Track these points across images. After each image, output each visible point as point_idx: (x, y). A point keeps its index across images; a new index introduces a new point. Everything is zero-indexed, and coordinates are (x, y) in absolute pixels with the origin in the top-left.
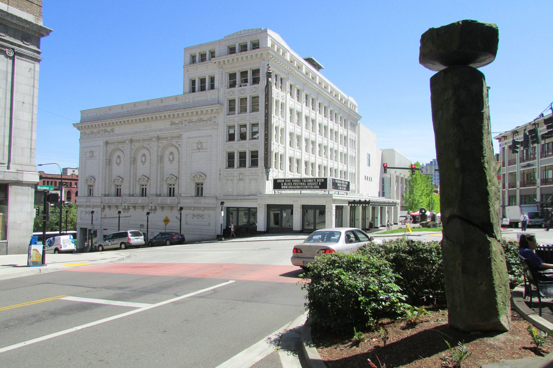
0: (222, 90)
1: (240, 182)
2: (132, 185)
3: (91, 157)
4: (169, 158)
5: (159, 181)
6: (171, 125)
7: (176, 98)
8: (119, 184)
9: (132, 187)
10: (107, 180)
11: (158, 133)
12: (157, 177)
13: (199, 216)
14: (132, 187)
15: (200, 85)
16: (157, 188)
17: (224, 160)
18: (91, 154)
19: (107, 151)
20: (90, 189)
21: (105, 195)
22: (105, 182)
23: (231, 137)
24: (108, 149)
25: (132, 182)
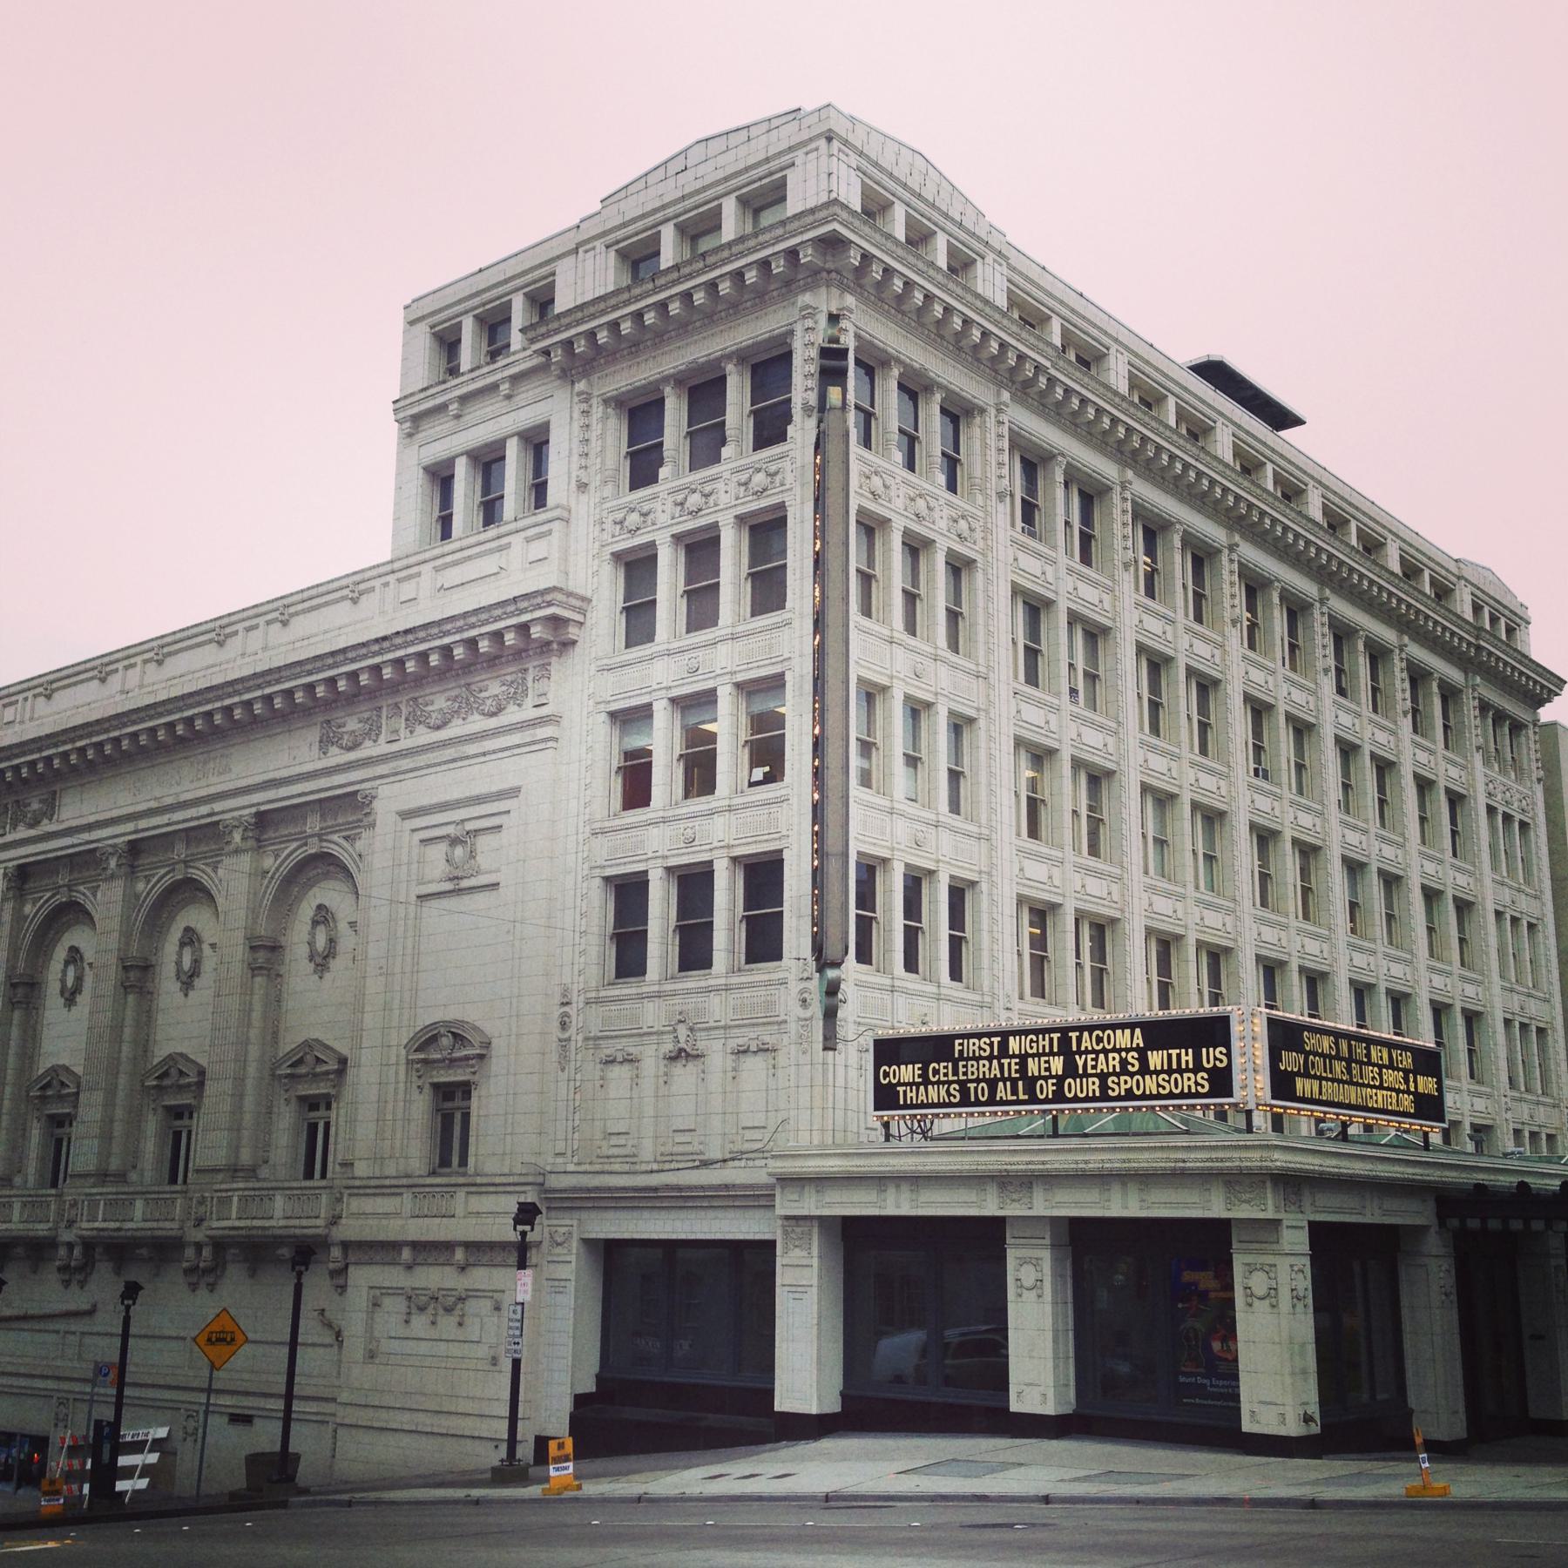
1: (678, 1069)
4: (311, 944)
7: (353, 589)
23: (635, 783)
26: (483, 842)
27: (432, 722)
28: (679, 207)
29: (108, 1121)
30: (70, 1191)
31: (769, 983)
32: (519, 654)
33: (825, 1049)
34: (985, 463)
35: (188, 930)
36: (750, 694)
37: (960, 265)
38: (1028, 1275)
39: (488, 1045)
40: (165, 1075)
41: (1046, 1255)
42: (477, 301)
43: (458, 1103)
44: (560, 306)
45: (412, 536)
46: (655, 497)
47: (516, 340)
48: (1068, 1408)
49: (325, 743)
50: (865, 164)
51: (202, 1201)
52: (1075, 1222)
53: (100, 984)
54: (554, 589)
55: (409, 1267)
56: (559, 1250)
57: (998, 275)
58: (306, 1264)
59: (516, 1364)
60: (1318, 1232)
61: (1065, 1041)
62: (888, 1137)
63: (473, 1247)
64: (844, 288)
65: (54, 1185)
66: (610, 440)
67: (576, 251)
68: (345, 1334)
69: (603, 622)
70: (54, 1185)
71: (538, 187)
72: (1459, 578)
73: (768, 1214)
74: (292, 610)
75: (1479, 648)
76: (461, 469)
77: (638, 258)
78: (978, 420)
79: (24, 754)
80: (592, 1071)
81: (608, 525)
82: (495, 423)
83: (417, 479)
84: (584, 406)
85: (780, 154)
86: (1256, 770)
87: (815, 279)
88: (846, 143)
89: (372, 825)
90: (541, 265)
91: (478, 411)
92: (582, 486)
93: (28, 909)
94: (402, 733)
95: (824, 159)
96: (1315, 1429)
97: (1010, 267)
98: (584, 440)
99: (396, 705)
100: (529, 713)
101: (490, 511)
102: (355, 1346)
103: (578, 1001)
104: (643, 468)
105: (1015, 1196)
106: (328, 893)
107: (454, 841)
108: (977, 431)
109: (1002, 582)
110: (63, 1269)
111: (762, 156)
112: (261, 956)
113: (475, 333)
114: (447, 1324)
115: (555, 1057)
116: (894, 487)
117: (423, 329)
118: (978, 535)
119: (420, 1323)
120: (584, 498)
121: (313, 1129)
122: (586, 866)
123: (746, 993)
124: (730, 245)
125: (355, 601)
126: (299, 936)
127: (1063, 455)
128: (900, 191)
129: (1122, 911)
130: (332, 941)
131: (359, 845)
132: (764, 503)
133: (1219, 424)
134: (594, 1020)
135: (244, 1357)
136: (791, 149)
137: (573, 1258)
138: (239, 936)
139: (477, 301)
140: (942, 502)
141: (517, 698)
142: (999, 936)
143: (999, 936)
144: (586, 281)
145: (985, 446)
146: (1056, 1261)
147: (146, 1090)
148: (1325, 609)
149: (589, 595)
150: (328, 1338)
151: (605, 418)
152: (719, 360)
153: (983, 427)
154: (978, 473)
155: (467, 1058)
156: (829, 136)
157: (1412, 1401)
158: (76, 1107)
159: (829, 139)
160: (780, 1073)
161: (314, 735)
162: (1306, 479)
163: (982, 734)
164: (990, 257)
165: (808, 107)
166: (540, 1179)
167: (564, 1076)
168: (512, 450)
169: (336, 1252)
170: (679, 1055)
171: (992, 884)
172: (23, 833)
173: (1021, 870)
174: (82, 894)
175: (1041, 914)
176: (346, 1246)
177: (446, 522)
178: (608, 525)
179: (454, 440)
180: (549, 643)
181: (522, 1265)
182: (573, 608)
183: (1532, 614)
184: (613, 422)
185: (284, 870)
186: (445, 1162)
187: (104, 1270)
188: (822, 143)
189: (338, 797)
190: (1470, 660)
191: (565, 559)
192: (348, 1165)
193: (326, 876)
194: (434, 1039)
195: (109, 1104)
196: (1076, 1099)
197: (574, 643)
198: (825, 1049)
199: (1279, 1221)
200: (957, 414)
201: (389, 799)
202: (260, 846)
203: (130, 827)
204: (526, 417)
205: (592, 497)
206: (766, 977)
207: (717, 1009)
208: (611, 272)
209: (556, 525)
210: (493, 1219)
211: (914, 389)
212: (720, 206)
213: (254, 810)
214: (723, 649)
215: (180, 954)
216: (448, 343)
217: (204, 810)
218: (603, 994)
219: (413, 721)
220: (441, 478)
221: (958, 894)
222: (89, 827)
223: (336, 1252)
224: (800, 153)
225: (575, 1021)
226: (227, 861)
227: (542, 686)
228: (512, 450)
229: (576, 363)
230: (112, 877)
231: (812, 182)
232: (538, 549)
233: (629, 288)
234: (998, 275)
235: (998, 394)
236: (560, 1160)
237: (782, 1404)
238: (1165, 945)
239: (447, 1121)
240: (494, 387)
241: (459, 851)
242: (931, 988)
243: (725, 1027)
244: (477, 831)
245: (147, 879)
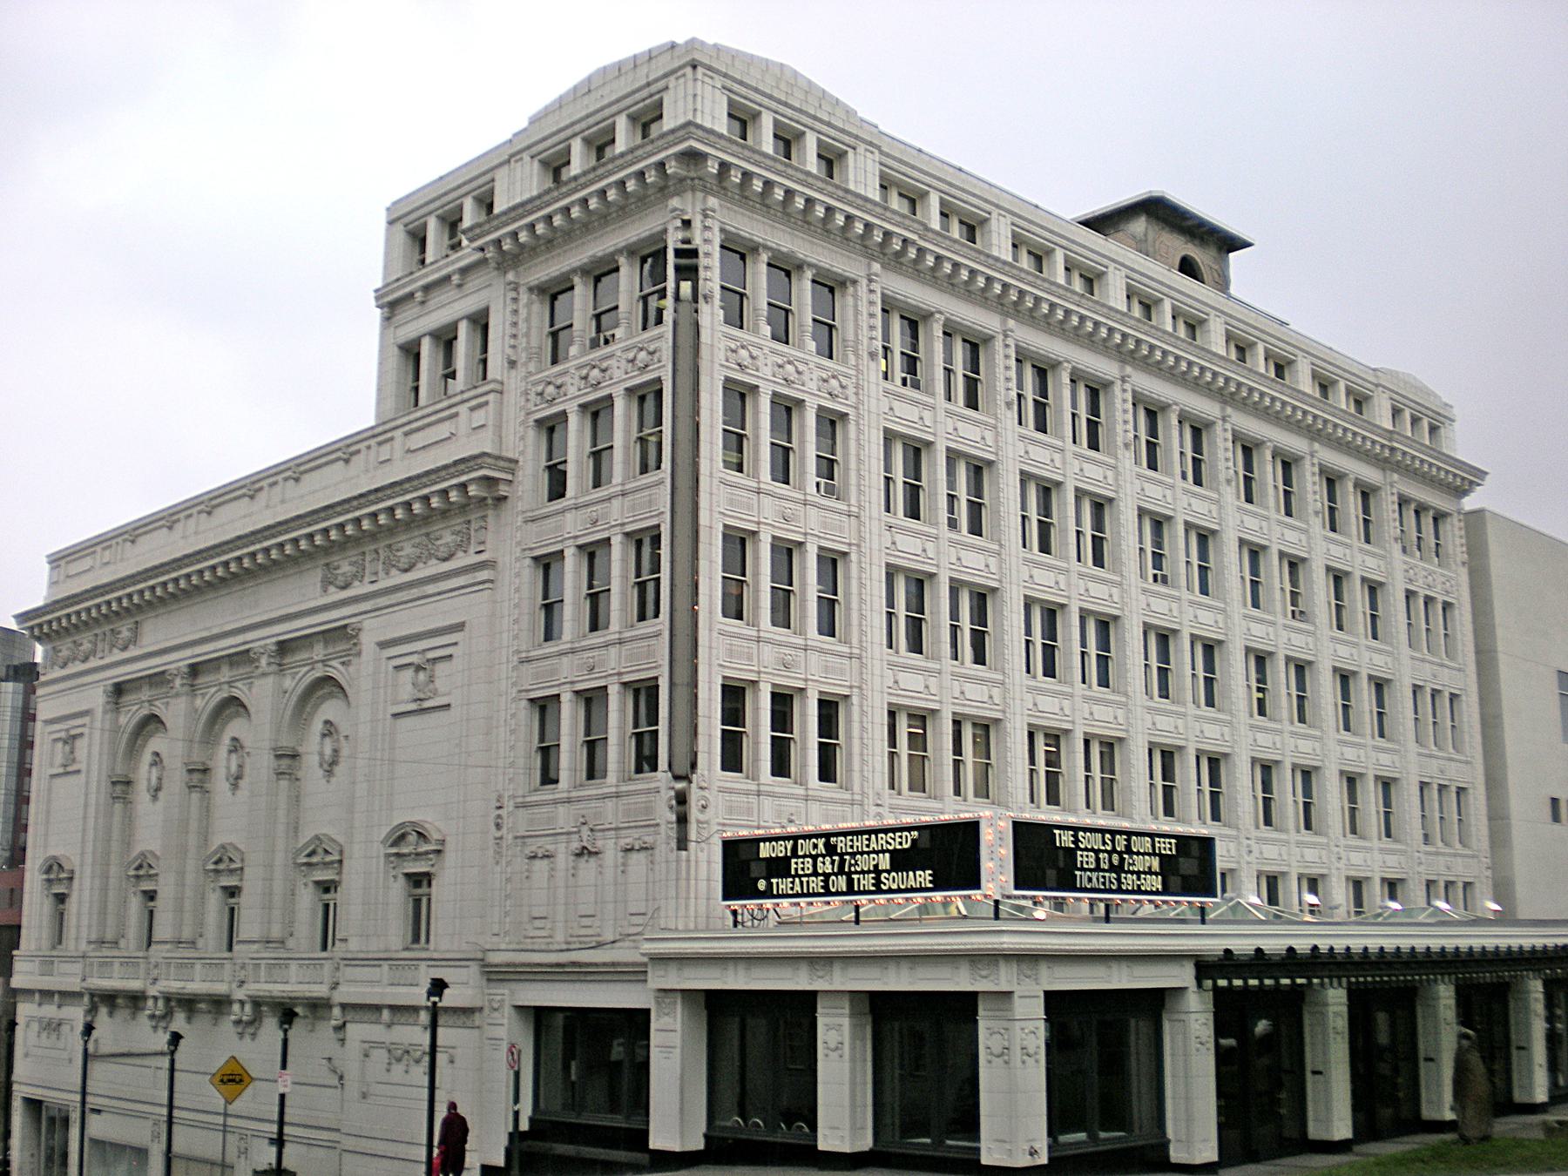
7: (344, 451)
19: (116, 729)
22: (105, 877)
26: (441, 668)
27: (440, 555)
28: (583, 125)
31: (648, 792)
32: (463, 508)
33: (679, 849)
34: (857, 326)
35: (235, 739)
37: (831, 160)
39: (443, 842)
40: (140, 867)
42: (438, 204)
46: (565, 373)
49: (327, 583)
50: (729, 83)
52: (874, 996)
53: (261, 764)
54: (484, 454)
55: (389, 1026)
56: (496, 1014)
57: (869, 162)
58: (290, 1023)
60: (1054, 1001)
62: (736, 923)
63: (63, 994)
64: (707, 191)
66: (535, 322)
67: (508, 161)
68: (346, 1077)
69: (530, 481)
71: (476, 106)
72: (1377, 385)
73: (639, 986)
74: (302, 468)
75: (1392, 449)
76: (426, 347)
77: (555, 167)
78: (851, 290)
79: (112, 591)
80: (520, 863)
81: (532, 397)
82: (451, 308)
84: (513, 294)
85: (657, 80)
86: (1155, 576)
87: (682, 185)
88: (710, 68)
89: (359, 654)
90: (484, 174)
91: (438, 298)
92: (512, 364)
93: (123, 720)
94: (382, 574)
95: (690, 84)
97: (881, 152)
98: (515, 321)
99: (376, 551)
100: (474, 559)
103: (509, 806)
105: (984, 973)
106: (331, 709)
107: (419, 668)
108: (850, 300)
109: (874, 431)
111: (644, 82)
112: (285, 762)
113: (438, 227)
115: (491, 852)
116: (761, 358)
117: (399, 227)
118: (851, 391)
119: (398, 1069)
120: (513, 372)
122: (515, 690)
123: (632, 800)
124: (622, 155)
125: (347, 461)
126: (313, 747)
127: (940, 313)
128: (766, 101)
129: (1004, 712)
130: (336, 751)
131: (351, 669)
133: (1111, 269)
134: (519, 822)
136: (666, 76)
137: (505, 1021)
138: (267, 744)
139: (438, 204)
140: (812, 365)
141: (462, 546)
144: (518, 186)
145: (857, 312)
146: (854, 1026)
147: (207, 871)
148: (1228, 426)
149: (516, 456)
151: (529, 304)
152: (613, 254)
153: (855, 297)
154: (851, 336)
155: (427, 853)
156: (691, 61)
157: (1170, 1133)
158: (340, 873)
159: (694, 67)
160: (657, 867)
161: (317, 575)
162: (1207, 309)
163: (854, 567)
164: (861, 148)
165: (680, 40)
166: (480, 955)
167: (498, 869)
168: (463, 329)
169: (336, 1011)
170: (583, 852)
171: (862, 697)
172: (118, 656)
173: (896, 682)
176: (344, 1006)
178: (532, 397)
179: (420, 323)
180: (485, 499)
182: (502, 470)
183: (1456, 412)
184: (536, 307)
185: (299, 690)
186: (416, 939)
188: (689, 70)
189: (335, 629)
190: (1386, 460)
191: (499, 427)
193: (331, 695)
194: (403, 837)
195: (181, 884)
196: (890, 891)
197: (505, 498)
198: (679, 849)
200: (830, 285)
201: (373, 631)
202: (282, 669)
203: (188, 652)
204: (470, 304)
205: (521, 371)
206: (646, 786)
207: (610, 813)
208: (535, 179)
209: (491, 397)
211: (785, 268)
212: (569, 147)
213: (274, 640)
214: (616, 503)
215: (228, 760)
216: (419, 239)
218: (574, 794)
219: (389, 565)
220: (411, 352)
221: (829, 710)
223: (336, 1011)
224: (672, 78)
225: (507, 823)
226: (257, 682)
227: (481, 535)
228: (463, 329)
229: (509, 259)
230: (177, 695)
231: (681, 103)
232: (479, 417)
233: (594, 169)
234: (869, 162)
235: (869, 266)
236: (495, 939)
237: (655, 1143)
239: (417, 902)
240: (447, 278)
241: (422, 676)
242: (800, 791)
243: (617, 829)
244: (435, 660)
245: (203, 695)
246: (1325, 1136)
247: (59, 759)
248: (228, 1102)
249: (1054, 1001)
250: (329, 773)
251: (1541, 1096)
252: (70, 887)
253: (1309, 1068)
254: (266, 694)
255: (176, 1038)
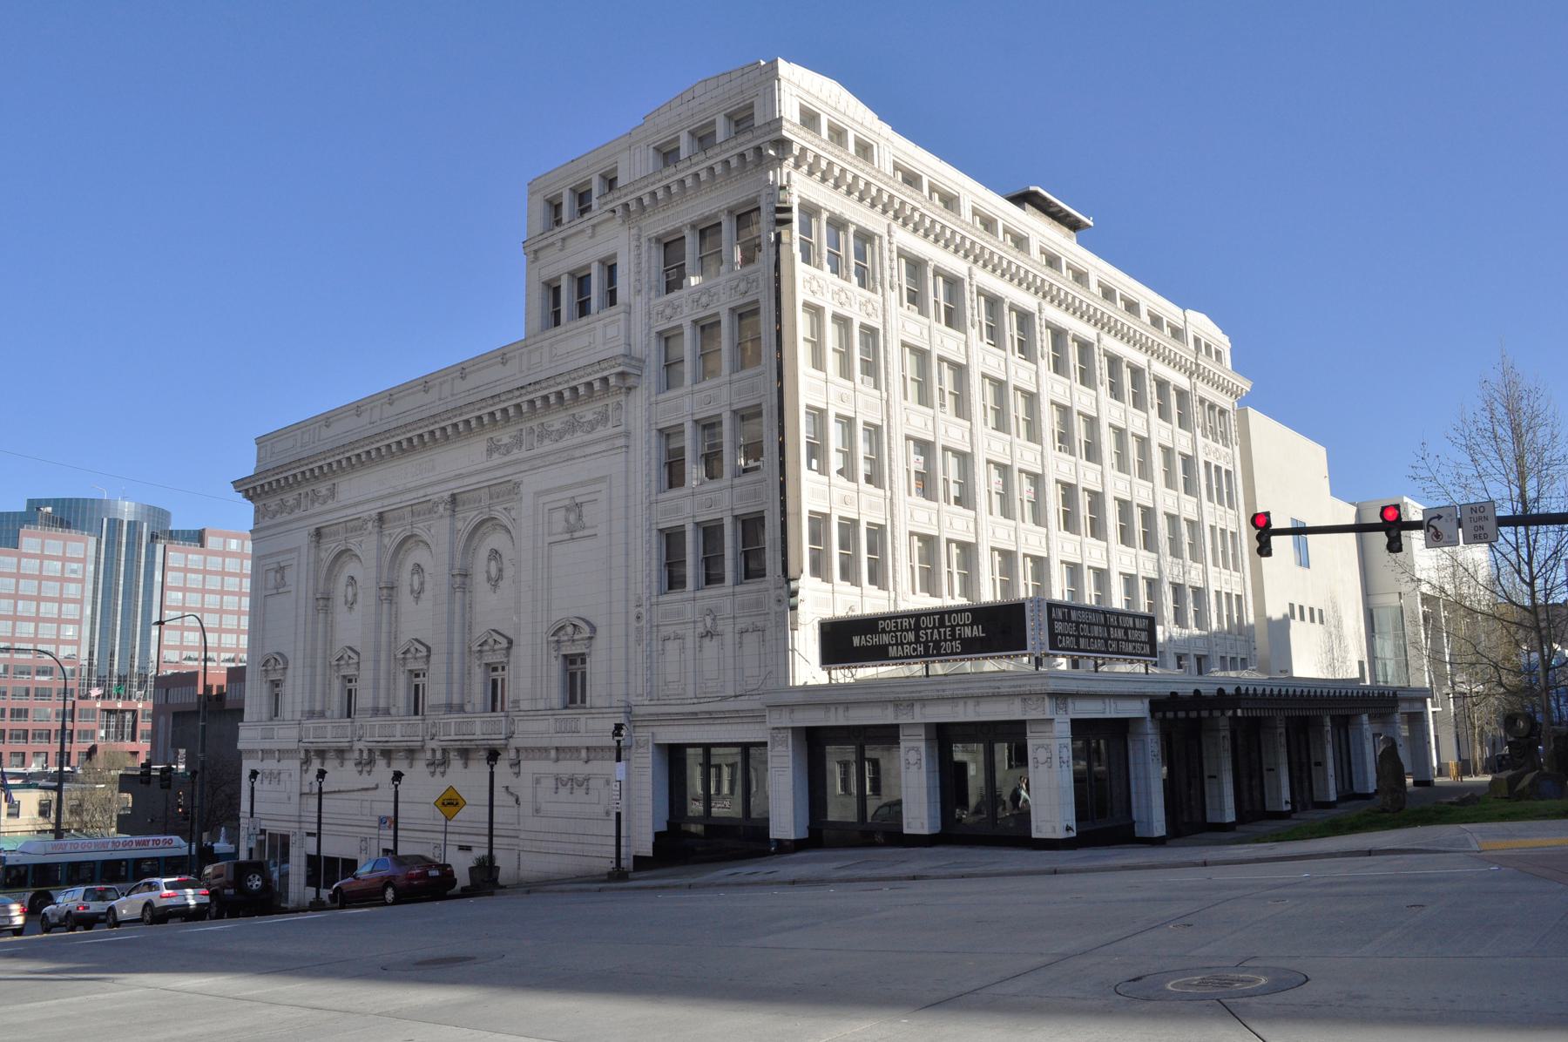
0: (639, 305)
1: (707, 641)
2: (383, 675)
3: (571, 530)
4: (488, 572)
5: (456, 656)
6: (490, 451)
7: (503, 356)
8: (350, 671)
9: (383, 683)
10: (319, 662)
11: (452, 485)
12: (451, 642)
13: (573, 782)
14: (383, 683)
15: (571, 297)
16: (450, 683)
17: (646, 560)
18: (572, 518)
19: (318, 561)
20: (495, 682)
21: (311, 714)
22: (313, 667)
23: (674, 473)
24: (323, 555)
25: (383, 665)
29: (376, 681)
30: (359, 719)
36: (743, 418)
38: (913, 757)
41: (922, 745)
43: (579, 665)
44: (620, 183)
45: (537, 323)
47: (595, 203)
48: (937, 830)
51: (434, 725)
58: (495, 760)
59: (618, 815)
60: (1079, 727)
61: (917, 622)
65: (349, 716)
66: (654, 262)
70: (349, 716)
83: (538, 291)
96: (1073, 834)
101: (583, 309)
102: (526, 808)
104: (673, 282)
106: (496, 540)
110: (358, 764)
114: (580, 792)
119: (564, 792)
121: (495, 682)
126: (481, 566)
132: (746, 300)
135: (463, 814)
142: (903, 560)
143: (903, 560)
146: (928, 747)
150: (512, 801)
157: (1135, 817)
170: (709, 634)
174: (353, 544)
175: (928, 542)
177: (557, 314)
181: (619, 759)
184: (654, 252)
185: (470, 528)
186: (573, 700)
187: (381, 763)
192: (516, 702)
195: (377, 669)
199: (1052, 720)
203: (379, 504)
210: (597, 730)
211: (838, 224)
216: (555, 207)
217: (421, 493)
222: (356, 505)
238: (1008, 557)
239: (573, 676)
246: (1218, 820)
247: (271, 583)
248: (447, 819)
249: (1079, 727)
250: (351, 608)
251: (1333, 797)
252: (284, 674)
253: (1206, 774)
254: (438, 531)
255: (398, 776)
